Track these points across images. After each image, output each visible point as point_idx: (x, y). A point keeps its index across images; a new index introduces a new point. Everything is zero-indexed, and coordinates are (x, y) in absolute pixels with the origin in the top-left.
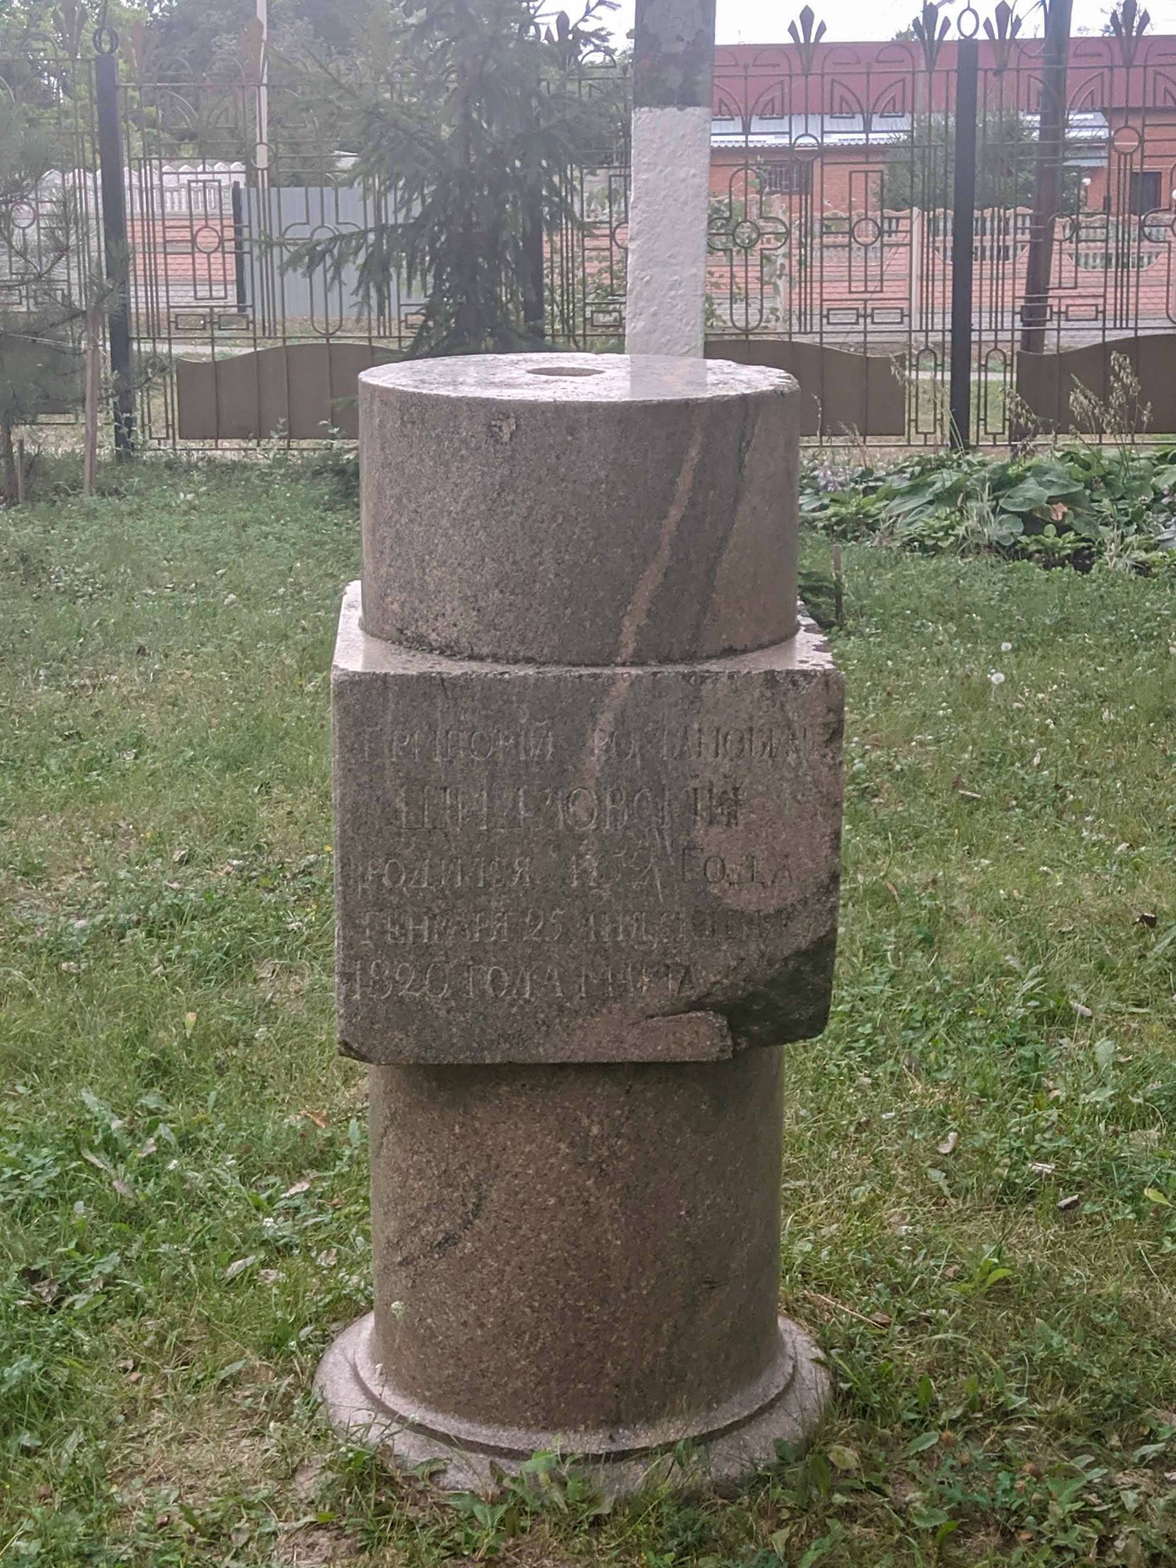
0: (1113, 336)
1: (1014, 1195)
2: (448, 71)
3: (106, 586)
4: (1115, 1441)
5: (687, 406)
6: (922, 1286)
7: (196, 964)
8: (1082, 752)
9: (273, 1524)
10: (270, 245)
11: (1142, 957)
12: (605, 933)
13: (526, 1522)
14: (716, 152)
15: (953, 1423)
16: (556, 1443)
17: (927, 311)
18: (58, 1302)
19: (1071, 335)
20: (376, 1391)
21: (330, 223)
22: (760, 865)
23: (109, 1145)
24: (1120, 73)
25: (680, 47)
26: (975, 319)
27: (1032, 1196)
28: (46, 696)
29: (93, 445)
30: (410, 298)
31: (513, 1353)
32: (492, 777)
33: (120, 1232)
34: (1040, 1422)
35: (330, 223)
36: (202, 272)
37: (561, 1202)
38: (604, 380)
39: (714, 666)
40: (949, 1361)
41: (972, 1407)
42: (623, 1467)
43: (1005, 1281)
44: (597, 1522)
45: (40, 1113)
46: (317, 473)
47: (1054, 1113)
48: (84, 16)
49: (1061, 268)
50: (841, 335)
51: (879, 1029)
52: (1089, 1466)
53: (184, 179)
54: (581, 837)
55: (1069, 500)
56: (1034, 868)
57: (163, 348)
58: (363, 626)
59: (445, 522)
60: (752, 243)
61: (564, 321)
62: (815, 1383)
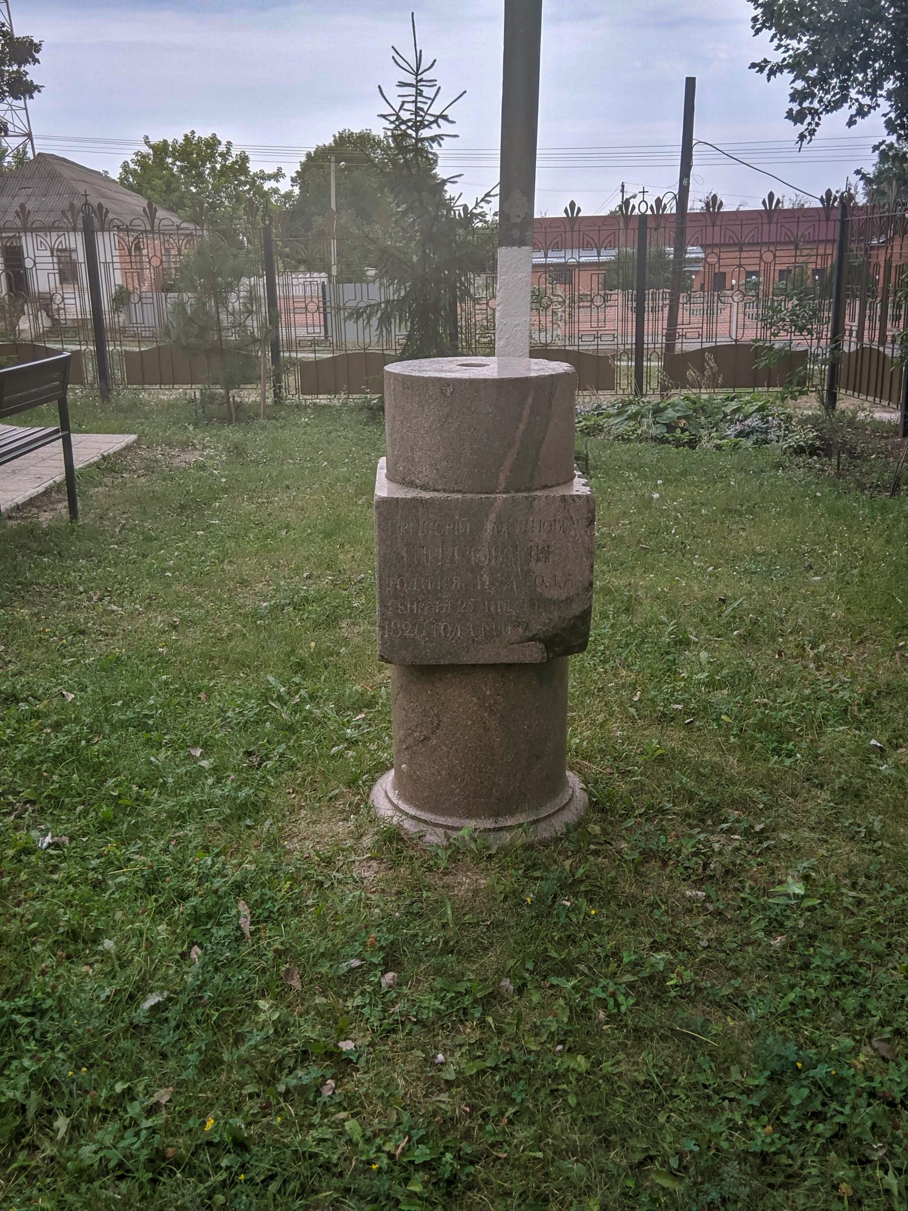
0: (705, 345)
1: (665, 719)
2: (416, 231)
3: (272, 459)
4: (710, 822)
5: (527, 380)
6: (626, 757)
7: (314, 621)
8: (693, 527)
9: (353, 857)
10: (340, 309)
11: (720, 616)
12: (492, 608)
13: (460, 857)
14: (535, 266)
15: (641, 815)
16: (472, 824)
17: (625, 335)
18: (260, 765)
19: (689, 345)
20: (396, 802)
21: (365, 299)
22: (559, 579)
23: (280, 699)
24: (766, 227)
25: (519, 220)
26: (645, 338)
27: (673, 719)
28: (248, 507)
29: (264, 398)
30: (400, 332)
31: (453, 786)
32: (443, 542)
33: (285, 736)
34: (678, 815)
35: (365, 299)
36: (310, 322)
37: (474, 723)
38: (489, 368)
39: (538, 493)
40: (639, 789)
41: (648, 808)
42: (501, 834)
43: (662, 755)
44: (490, 857)
45: (250, 685)
46: (361, 409)
47: (682, 684)
48: (258, 209)
49: (683, 315)
50: (587, 346)
51: (607, 648)
52: (699, 833)
53: (301, 281)
54: (482, 568)
55: (686, 417)
56: (673, 579)
57: (294, 355)
58: (387, 477)
59: (422, 432)
60: (549, 306)
61: (467, 342)
62: (581, 798)
